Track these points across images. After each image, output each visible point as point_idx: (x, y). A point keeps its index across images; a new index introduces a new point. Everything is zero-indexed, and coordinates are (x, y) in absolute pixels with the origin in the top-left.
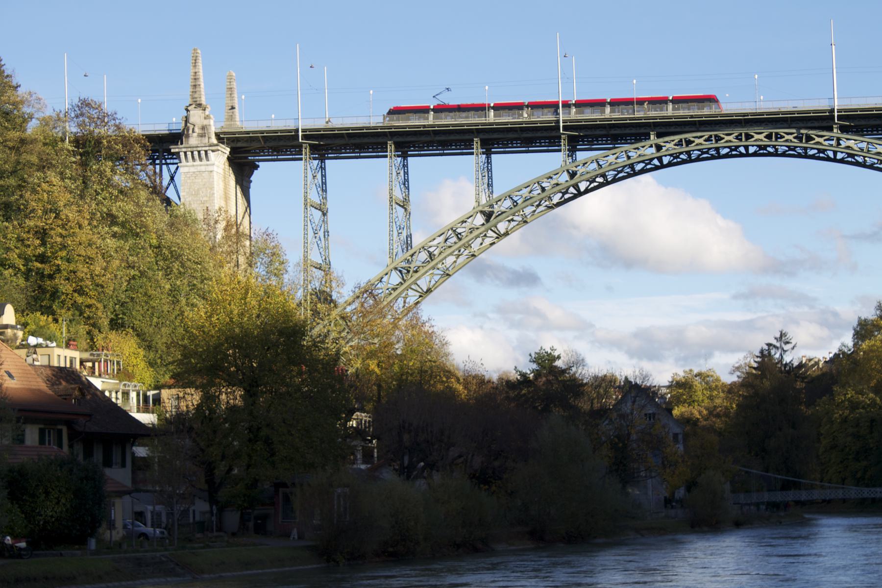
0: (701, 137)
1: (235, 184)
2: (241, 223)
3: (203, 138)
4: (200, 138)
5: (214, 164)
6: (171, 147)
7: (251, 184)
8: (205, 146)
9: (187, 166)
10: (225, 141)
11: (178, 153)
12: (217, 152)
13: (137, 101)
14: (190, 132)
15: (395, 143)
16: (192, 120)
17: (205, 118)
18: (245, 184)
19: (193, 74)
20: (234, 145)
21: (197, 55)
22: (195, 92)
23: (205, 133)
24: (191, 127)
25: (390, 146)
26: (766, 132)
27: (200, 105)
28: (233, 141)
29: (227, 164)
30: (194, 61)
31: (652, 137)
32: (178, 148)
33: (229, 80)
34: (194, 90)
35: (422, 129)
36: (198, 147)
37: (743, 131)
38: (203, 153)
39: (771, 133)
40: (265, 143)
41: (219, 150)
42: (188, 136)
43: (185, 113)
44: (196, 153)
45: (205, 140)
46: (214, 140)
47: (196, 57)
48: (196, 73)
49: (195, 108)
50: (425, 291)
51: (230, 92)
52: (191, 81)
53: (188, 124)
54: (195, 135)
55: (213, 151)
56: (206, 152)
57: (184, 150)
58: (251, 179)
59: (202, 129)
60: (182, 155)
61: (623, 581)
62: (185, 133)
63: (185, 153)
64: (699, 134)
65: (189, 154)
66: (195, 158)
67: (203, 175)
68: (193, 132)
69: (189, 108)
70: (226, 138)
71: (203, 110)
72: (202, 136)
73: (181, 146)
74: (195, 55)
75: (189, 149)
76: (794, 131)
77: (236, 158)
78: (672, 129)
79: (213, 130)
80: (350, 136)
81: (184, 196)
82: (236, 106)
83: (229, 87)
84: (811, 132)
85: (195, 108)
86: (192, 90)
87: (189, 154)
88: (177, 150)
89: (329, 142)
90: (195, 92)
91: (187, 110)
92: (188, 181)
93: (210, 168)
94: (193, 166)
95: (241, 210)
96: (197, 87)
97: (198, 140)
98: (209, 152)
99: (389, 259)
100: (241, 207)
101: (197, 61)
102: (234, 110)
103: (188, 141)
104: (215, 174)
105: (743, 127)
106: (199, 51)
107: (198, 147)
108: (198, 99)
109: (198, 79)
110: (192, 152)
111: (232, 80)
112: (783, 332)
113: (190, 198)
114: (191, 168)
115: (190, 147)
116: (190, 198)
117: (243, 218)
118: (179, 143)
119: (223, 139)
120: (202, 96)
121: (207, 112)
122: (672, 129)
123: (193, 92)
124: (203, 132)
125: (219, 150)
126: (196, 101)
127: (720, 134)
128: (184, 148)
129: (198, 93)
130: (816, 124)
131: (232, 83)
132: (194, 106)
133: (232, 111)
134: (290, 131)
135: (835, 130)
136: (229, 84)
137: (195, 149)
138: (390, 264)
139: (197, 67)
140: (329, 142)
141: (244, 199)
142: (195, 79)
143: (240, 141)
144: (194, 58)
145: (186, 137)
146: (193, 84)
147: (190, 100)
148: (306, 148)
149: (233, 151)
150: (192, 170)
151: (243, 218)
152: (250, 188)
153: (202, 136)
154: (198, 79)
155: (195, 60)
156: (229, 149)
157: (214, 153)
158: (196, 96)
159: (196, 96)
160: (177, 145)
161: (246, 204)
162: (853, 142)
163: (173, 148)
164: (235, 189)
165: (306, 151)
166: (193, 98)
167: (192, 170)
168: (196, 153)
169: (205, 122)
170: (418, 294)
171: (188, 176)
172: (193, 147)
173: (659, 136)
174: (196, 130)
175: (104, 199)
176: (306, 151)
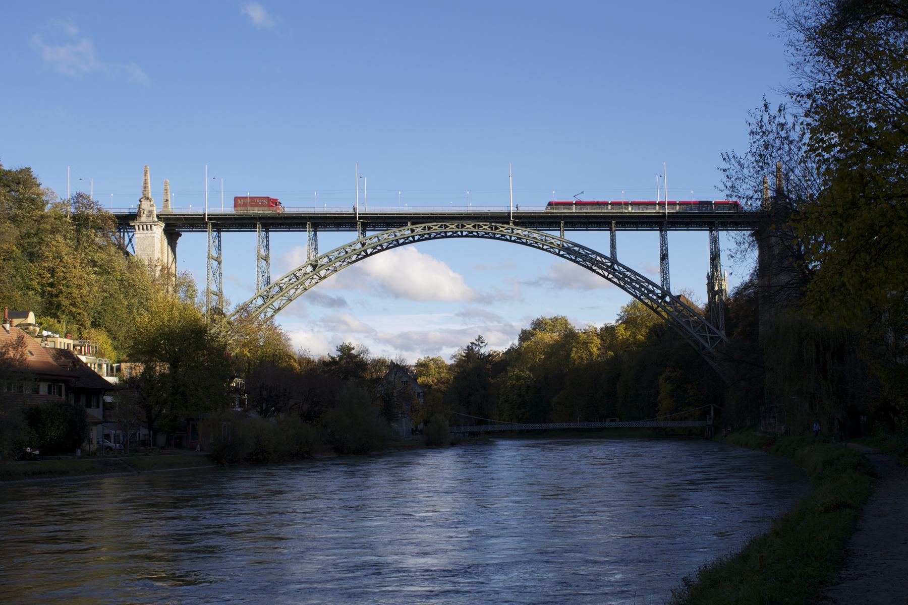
0: (436, 225)
5: (155, 233)
6: (130, 222)
11: (134, 226)
14: (142, 213)
15: (261, 223)
17: (151, 206)
20: (167, 222)
24: (142, 211)
26: (473, 224)
29: (163, 233)
31: (409, 224)
37: (460, 223)
38: (149, 226)
39: (476, 225)
42: (140, 216)
43: (139, 203)
44: (145, 226)
45: (151, 219)
48: (146, 180)
54: (145, 215)
55: (155, 225)
56: (151, 225)
58: (177, 242)
60: (137, 227)
63: (138, 226)
64: (435, 224)
65: (141, 226)
69: (141, 200)
72: (148, 217)
76: (488, 224)
78: (421, 221)
79: (155, 213)
84: (498, 225)
87: (141, 226)
91: (140, 201)
93: (153, 235)
94: (143, 233)
105: (460, 220)
110: (143, 226)
117: (172, 264)
119: (161, 218)
122: (421, 221)
127: (448, 224)
130: (501, 221)
135: (511, 224)
150: (142, 236)
151: (172, 264)
153: (148, 216)
156: (164, 225)
158: (146, 193)
159: (146, 193)
162: (520, 231)
167: (142, 236)
168: (145, 226)
169: (151, 208)
173: (413, 224)
174: (145, 213)
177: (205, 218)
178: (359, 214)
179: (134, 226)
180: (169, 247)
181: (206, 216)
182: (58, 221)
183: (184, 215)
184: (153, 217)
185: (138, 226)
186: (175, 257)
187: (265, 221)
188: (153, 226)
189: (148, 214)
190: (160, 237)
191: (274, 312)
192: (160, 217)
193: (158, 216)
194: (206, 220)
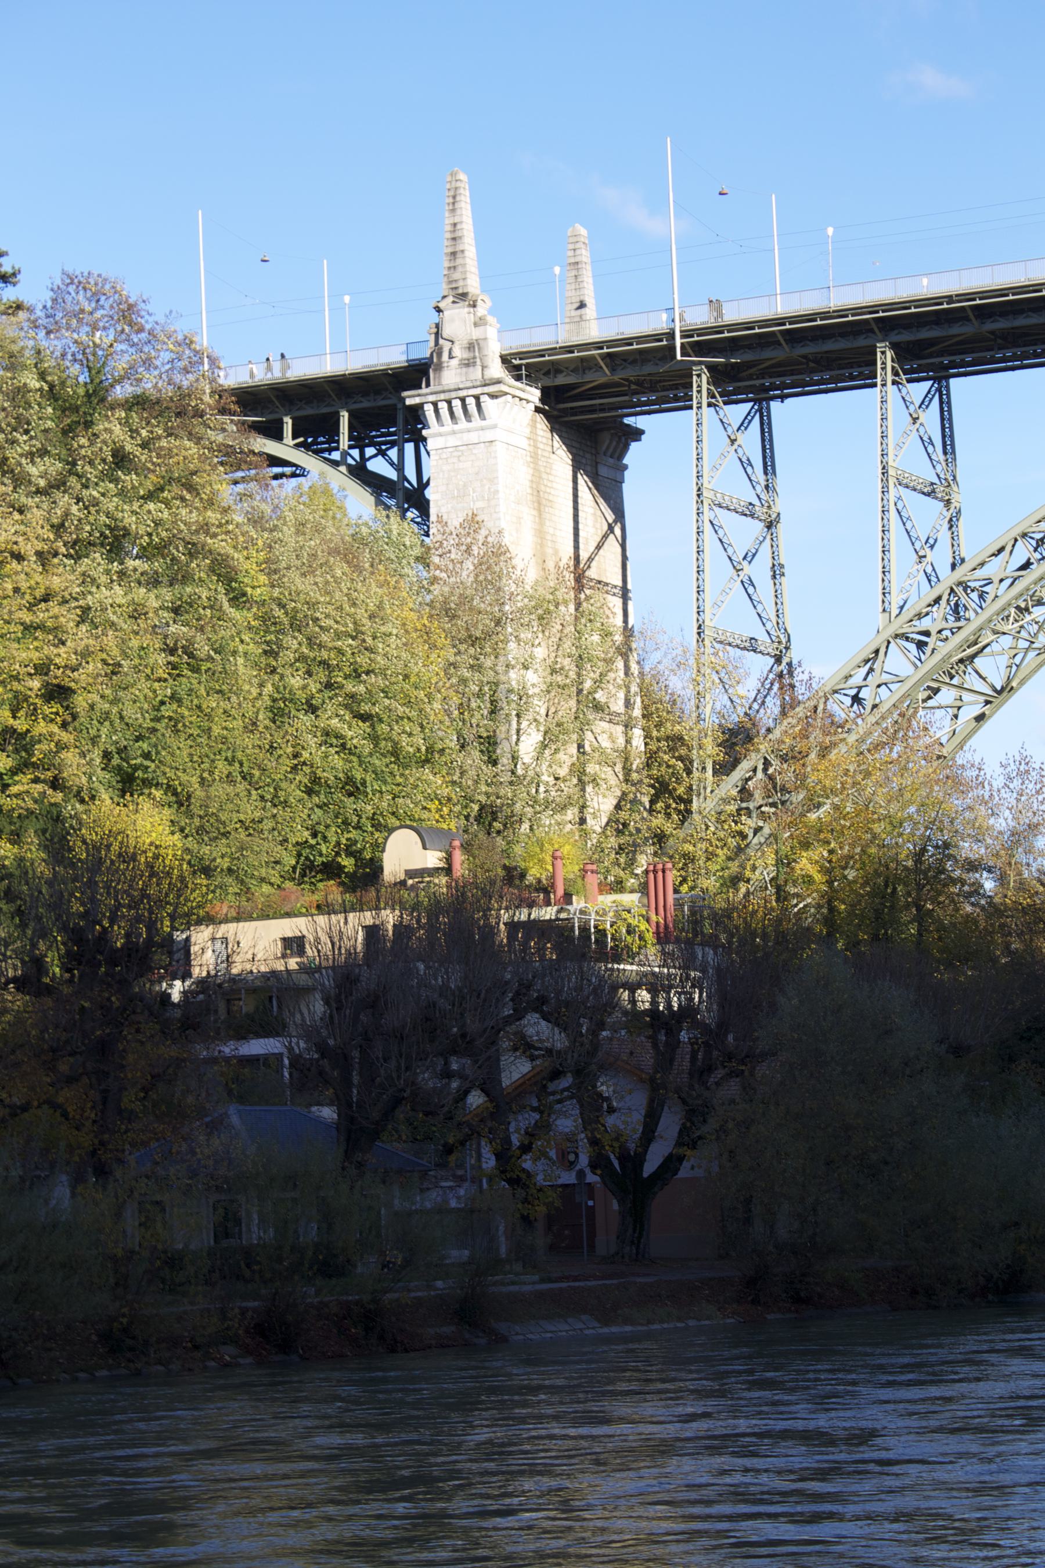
1: (569, 471)
2: (590, 559)
3: (471, 369)
4: (464, 370)
5: (495, 427)
6: (405, 394)
7: (626, 473)
8: (474, 387)
9: (441, 435)
10: (524, 372)
11: (420, 406)
12: (504, 398)
13: (343, 300)
14: (445, 356)
15: (894, 346)
16: (446, 332)
17: (476, 325)
18: (603, 471)
19: (449, 228)
20: (549, 382)
21: (458, 184)
22: (455, 267)
23: (474, 358)
24: (446, 346)
25: (883, 353)
27: (464, 296)
28: (547, 373)
29: (542, 424)
30: (451, 200)
32: (419, 395)
33: (571, 246)
34: (452, 265)
35: (945, 306)
36: (460, 389)
38: (471, 402)
40: (613, 370)
41: (506, 394)
42: (439, 367)
43: (435, 317)
44: (457, 404)
45: (476, 374)
46: (497, 370)
47: (456, 188)
48: (455, 225)
49: (454, 302)
50: (999, 688)
51: (574, 273)
52: (446, 243)
53: (441, 341)
54: (454, 362)
55: (493, 396)
56: (477, 398)
57: (432, 398)
58: (625, 461)
59: (469, 348)
60: (429, 409)
61: (1029, 1451)
62: (435, 360)
63: (435, 404)
65: (443, 406)
66: (456, 414)
67: (475, 451)
68: (451, 357)
69: (442, 305)
70: (527, 365)
71: (470, 306)
72: (467, 365)
73: (428, 390)
74: (454, 185)
75: (442, 396)
77: (565, 412)
79: (494, 349)
80: (794, 337)
81: (437, 501)
82: (590, 301)
83: (572, 260)
85: (454, 302)
86: (447, 264)
87: (443, 406)
88: (417, 400)
89: (749, 356)
90: (455, 267)
91: (439, 310)
92: (445, 468)
93: (488, 435)
94: (454, 433)
95: (592, 530)
96: (459, 255)
97: (461, 374)
98: (483, 398)
99: (880, 616)
100: (590, 522)
101: (458, 199)
102: (583, 311)
103: (440, 378)
104: (499, 448)
106: (462, 176)
107: (460, 389)
108: (461, 283)
109: (460, 237)
110: (449, 402)
111: (578, 246)
112: (477, 519)
113: (449, 506)
114: (449, 438)
115: (444, 392)
116: (449, 506)
117: (599, 547)
118: (424, 385)
119: (518, 368)
120: (468, 275)
121: (481, 310)
123: (449, 268)
124: (472, 355)
125: (506, 394)
126: (456, 288)
128: (432, 394)
129: (460, 269)
131: (578, 252)
132: (451, 299)
133: (579, 311)
134: (657, 337)
136: (571, 253)
137: (453, 395)
138: (884, 628)
139: (458, 212)
140: (749, 356)
141: (601, 501)
142: (454, 239)
143: (561, 372)
144: (452, 193)
145: (435, 370)
146: (450, 250)
147: (444, 286)
148: (699, 376)
149: (546, 395)
150: (452, 441)
151: (599, 547)
152: (623, 482)
153: (468, 364)
154: (460, 237)
155: (454, 197)
156: (538, 393)
157: (495, 401)
158: (456, 276)
159: (456, 276)
160: (420, 388)
161: (611, 517)
163: (409, 397)
164: (571, 484)
165: (702, 382)
166: (450, 282)
167: (452, 441)
168: (457, 404)
169: (476, 334)
170: (982, 699)
171: (444, 456)
172: (450, 391)
174: (457, 352)
175: (103, 495)
176: (702, 382)
177: (674, 348)
178: (686, 334)
179: (420, 406)
180: (583, 481)
181: (678, 342)
182: (802, 1294)
183: (780, 321)
184: (483, 367)
185: (435, 404)
186: (620, 515)
187: (905, 337)
188: (484, 399)
189: (466, 355)
190: (524, 443)
191: (987, 702)
192: (516, 362)
193: (505, 360)
194: (679, 357)
